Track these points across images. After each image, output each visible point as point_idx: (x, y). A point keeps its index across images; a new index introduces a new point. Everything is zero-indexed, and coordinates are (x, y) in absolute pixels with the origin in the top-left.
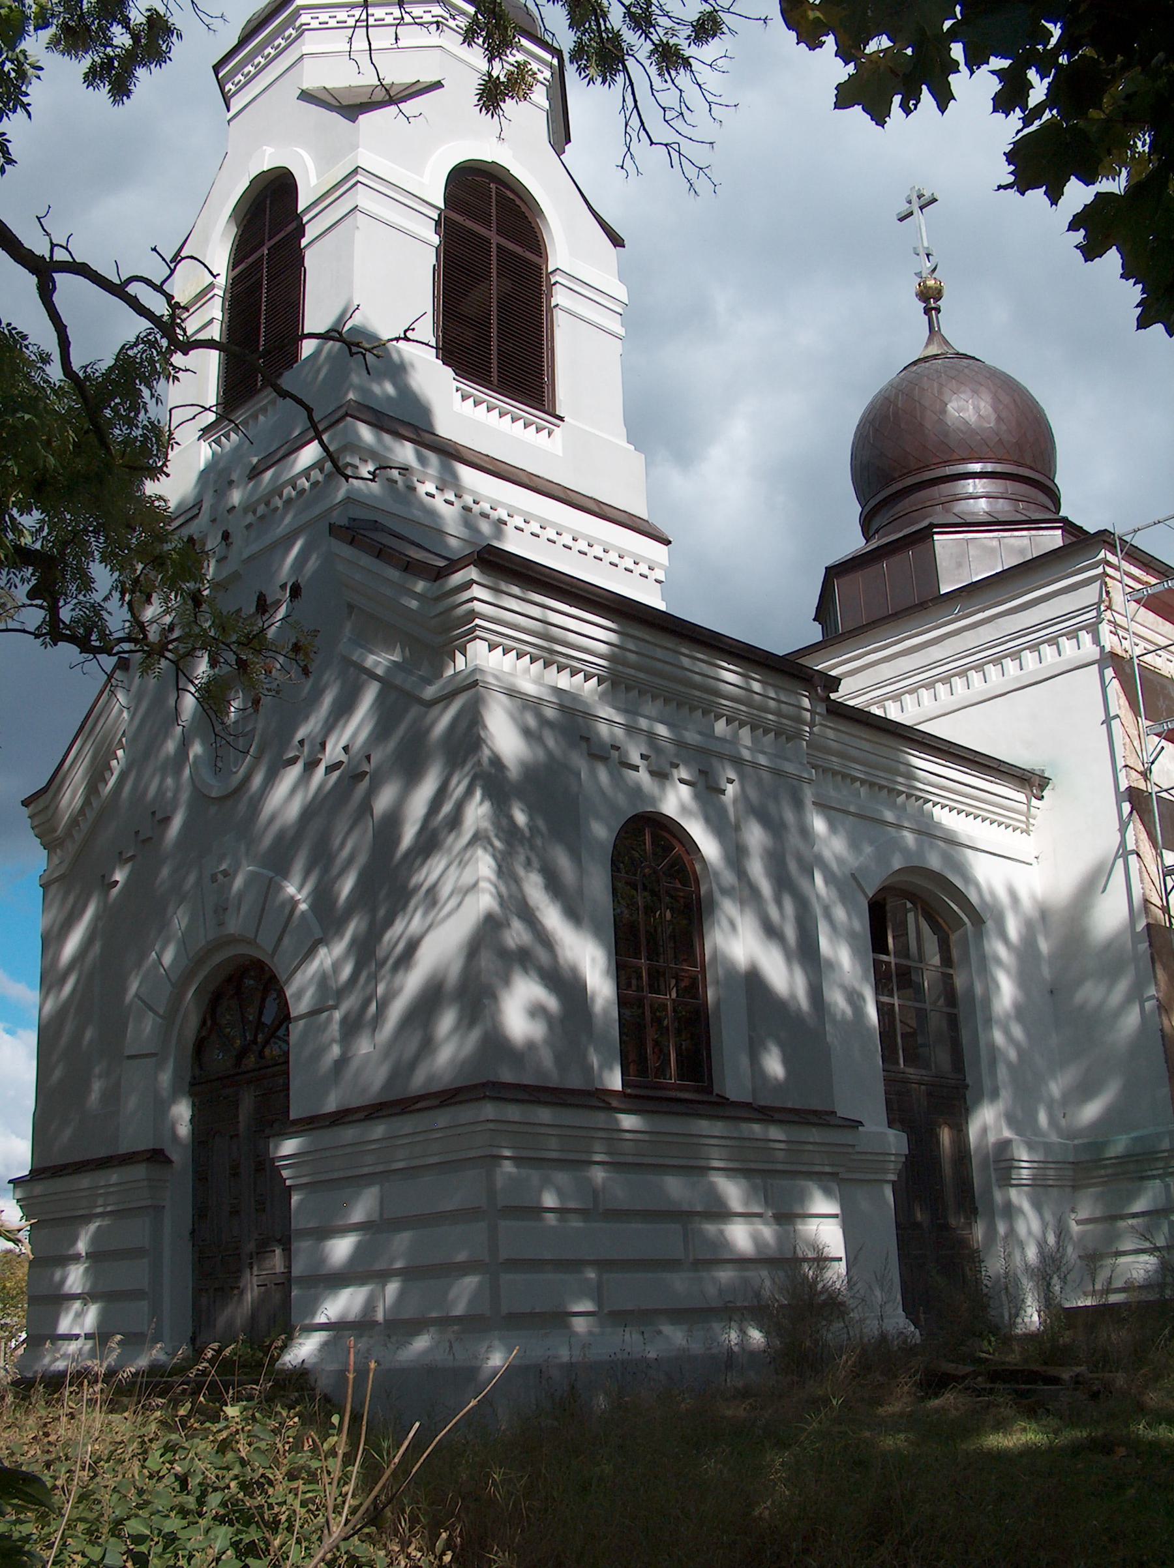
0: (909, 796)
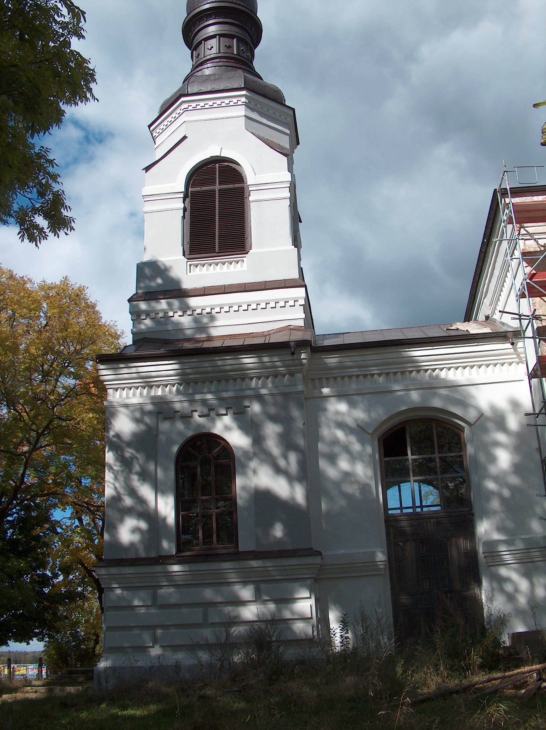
0: (418, 371)
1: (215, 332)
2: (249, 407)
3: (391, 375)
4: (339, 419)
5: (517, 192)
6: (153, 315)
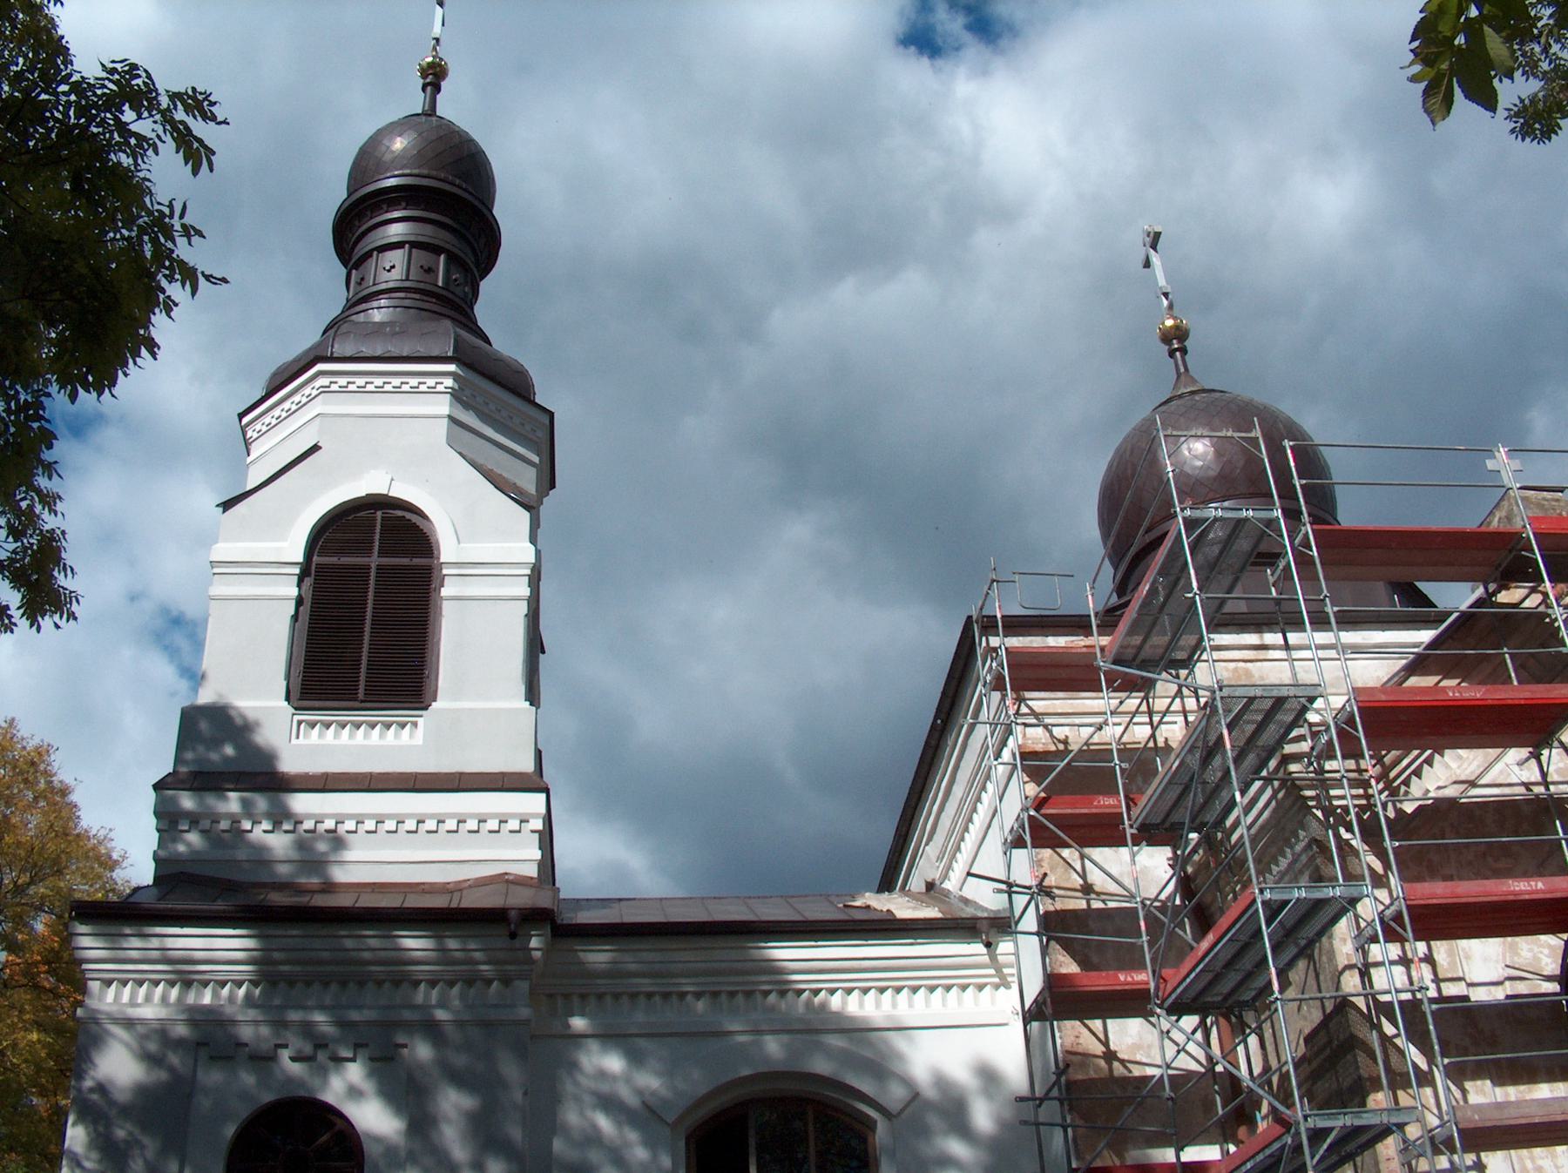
0: (783, 993)
1: (340, 875)
2: (405, 1046)
3: (724, 997)
4: (605, 1088)
5: (1016, 625)
6: (206, 824)
